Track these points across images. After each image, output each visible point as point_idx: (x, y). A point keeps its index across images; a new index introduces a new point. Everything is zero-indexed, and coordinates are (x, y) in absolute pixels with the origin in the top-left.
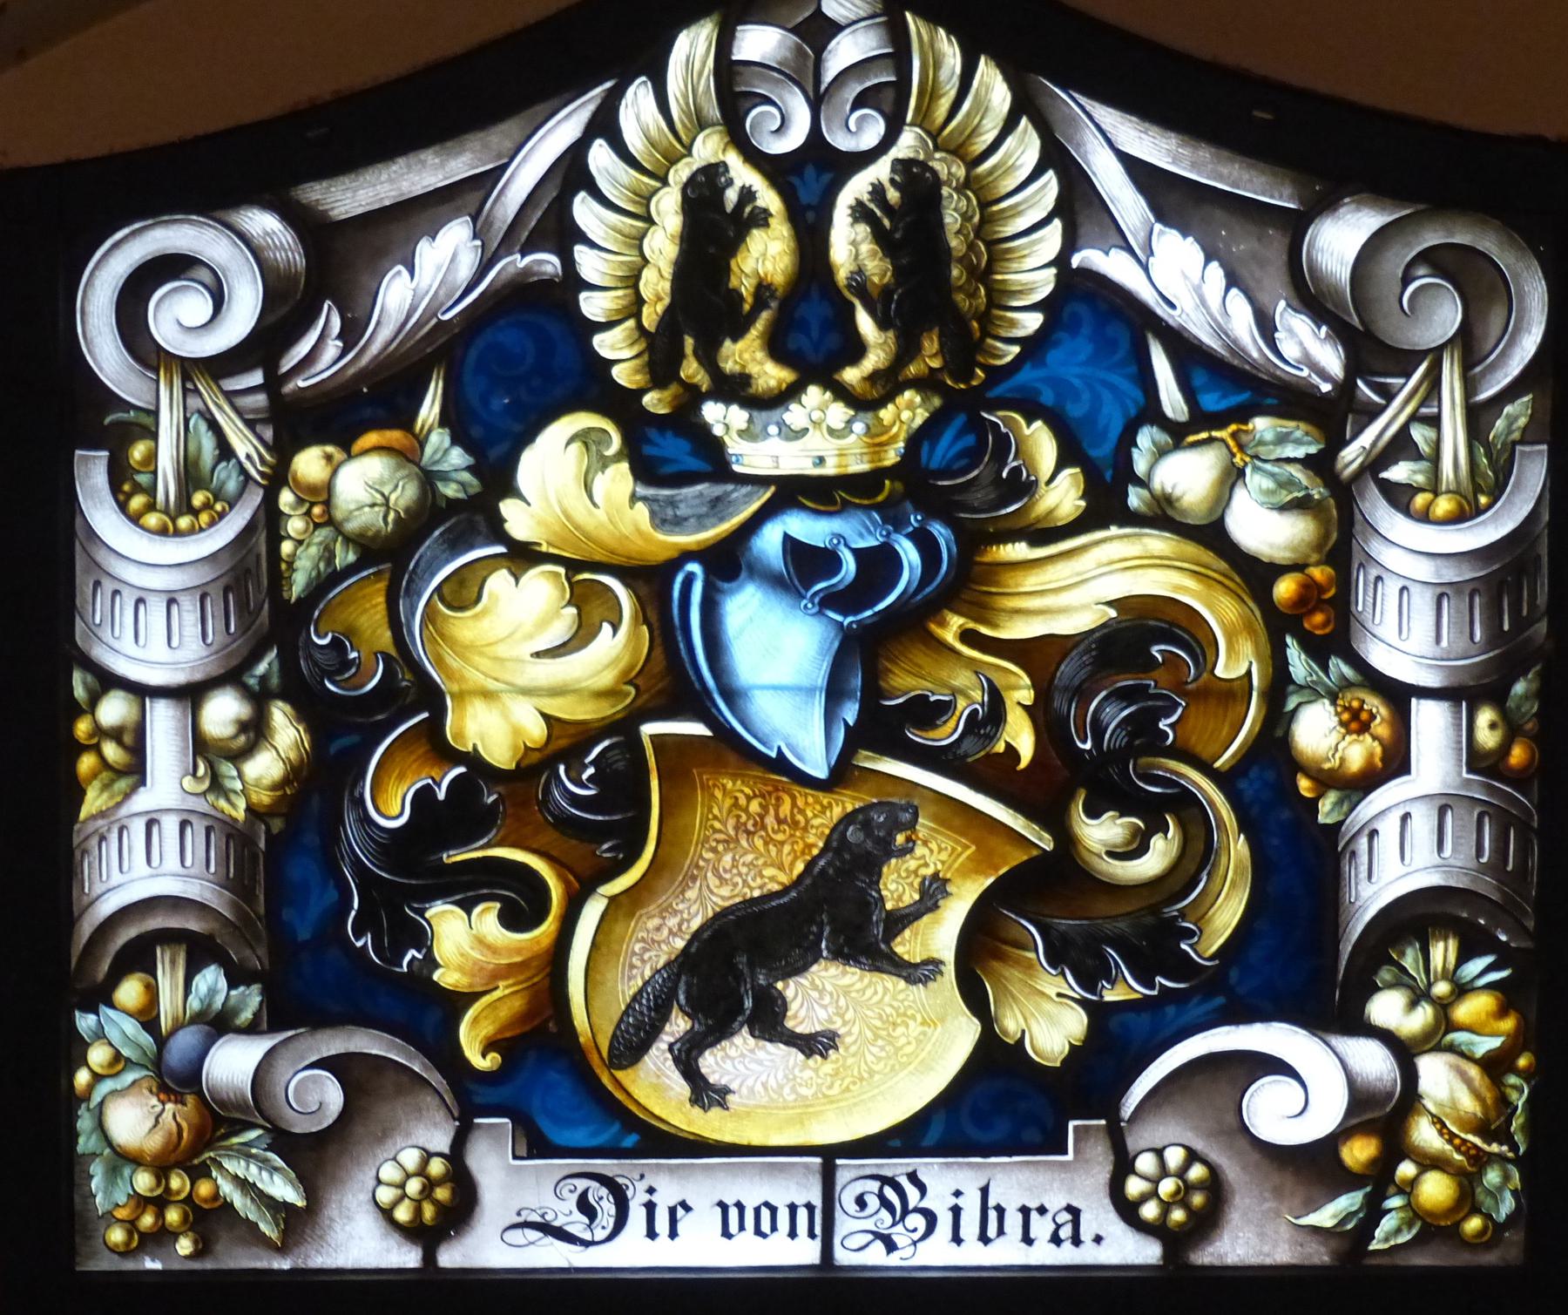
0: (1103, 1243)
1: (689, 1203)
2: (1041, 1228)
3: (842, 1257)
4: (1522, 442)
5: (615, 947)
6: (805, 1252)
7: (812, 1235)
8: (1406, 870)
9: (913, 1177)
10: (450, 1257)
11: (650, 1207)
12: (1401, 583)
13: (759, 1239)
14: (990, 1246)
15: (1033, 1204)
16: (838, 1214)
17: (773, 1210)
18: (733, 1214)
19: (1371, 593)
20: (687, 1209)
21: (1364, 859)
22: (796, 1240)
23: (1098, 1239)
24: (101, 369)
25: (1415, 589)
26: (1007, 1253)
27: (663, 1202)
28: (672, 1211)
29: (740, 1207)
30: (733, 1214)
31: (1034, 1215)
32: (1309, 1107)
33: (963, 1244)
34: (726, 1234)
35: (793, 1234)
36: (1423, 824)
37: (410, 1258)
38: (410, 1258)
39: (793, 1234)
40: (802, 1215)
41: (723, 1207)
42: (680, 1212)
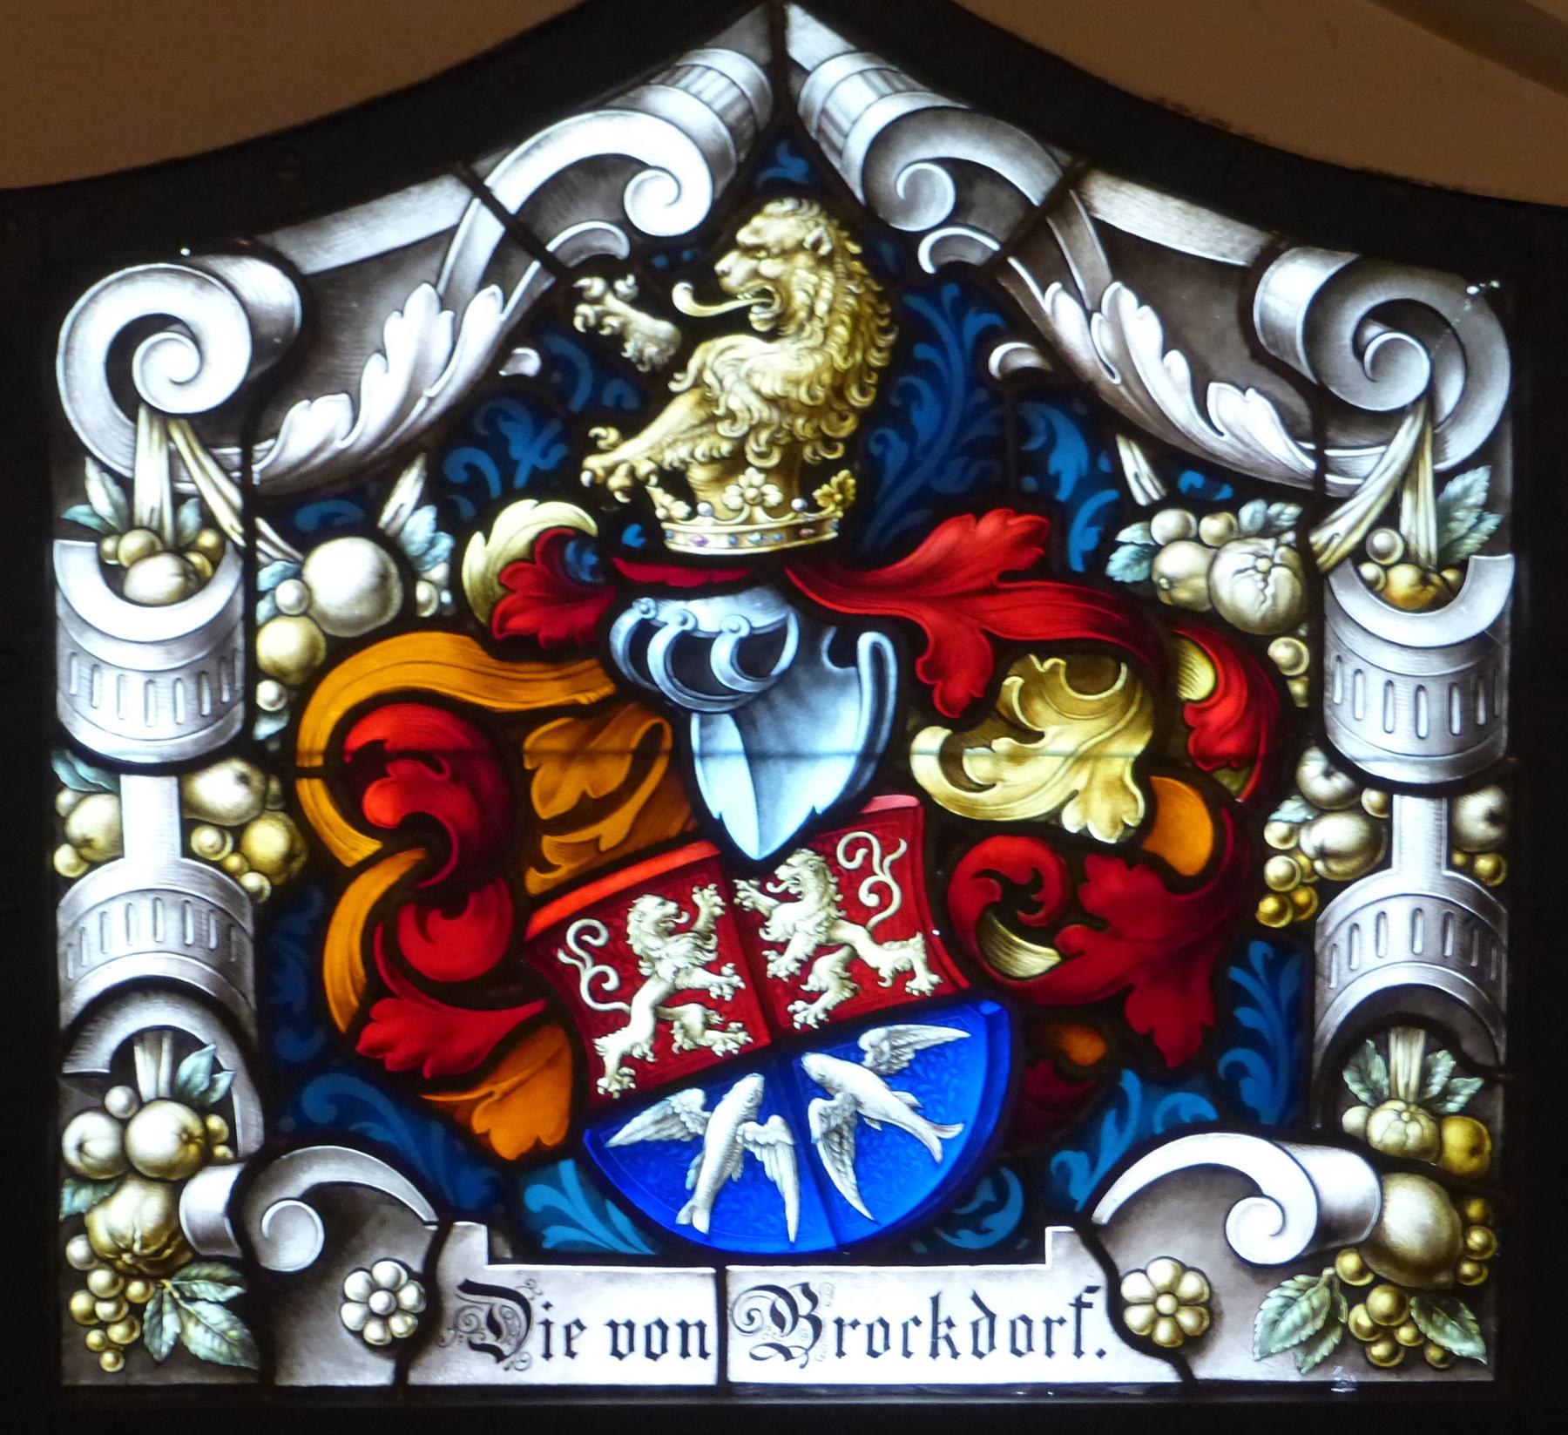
0: (1105, 1357)
1: (584, 1323)
2: (855, 1340)
3: (736, 1374)
4: (1479, 553)
5: (1326, 973)
6: (701, 1373)
7: (704, 1354)
8: (1381, 962)
9: (806, 1290)
10: (1207, 1369)
11: (547, 1324)
12: (1385, 677)
13: (615, 1359)
14: (985, 1358)
15: (1054, 1317)
16: (732, 1331)
17: (664, 1328)
18: (623, 1332)
19: (1349, 685)
20: (582, 1327)
21: (1343, 946)
22: (552, 1359)
23: (1101, 1354)
24: (70, 399)
25: (1397, 681)
26: (1000, 1369)
27: (560, 1319)
28: (568, 1328)
29: (630, 1325)
30: (623, 1332)
31: (1055, 1326)
32: (1283, 1204)
33: (1083, 1357)
34: (616, 1353)
35: (685, 1353)
36: (1399, 913)
37: (1162, 1372)
38: (1162, 1372)
39: (685, 1353)
40: (694, 1333)
41: (613, 1325)
42: (575, 1331)
